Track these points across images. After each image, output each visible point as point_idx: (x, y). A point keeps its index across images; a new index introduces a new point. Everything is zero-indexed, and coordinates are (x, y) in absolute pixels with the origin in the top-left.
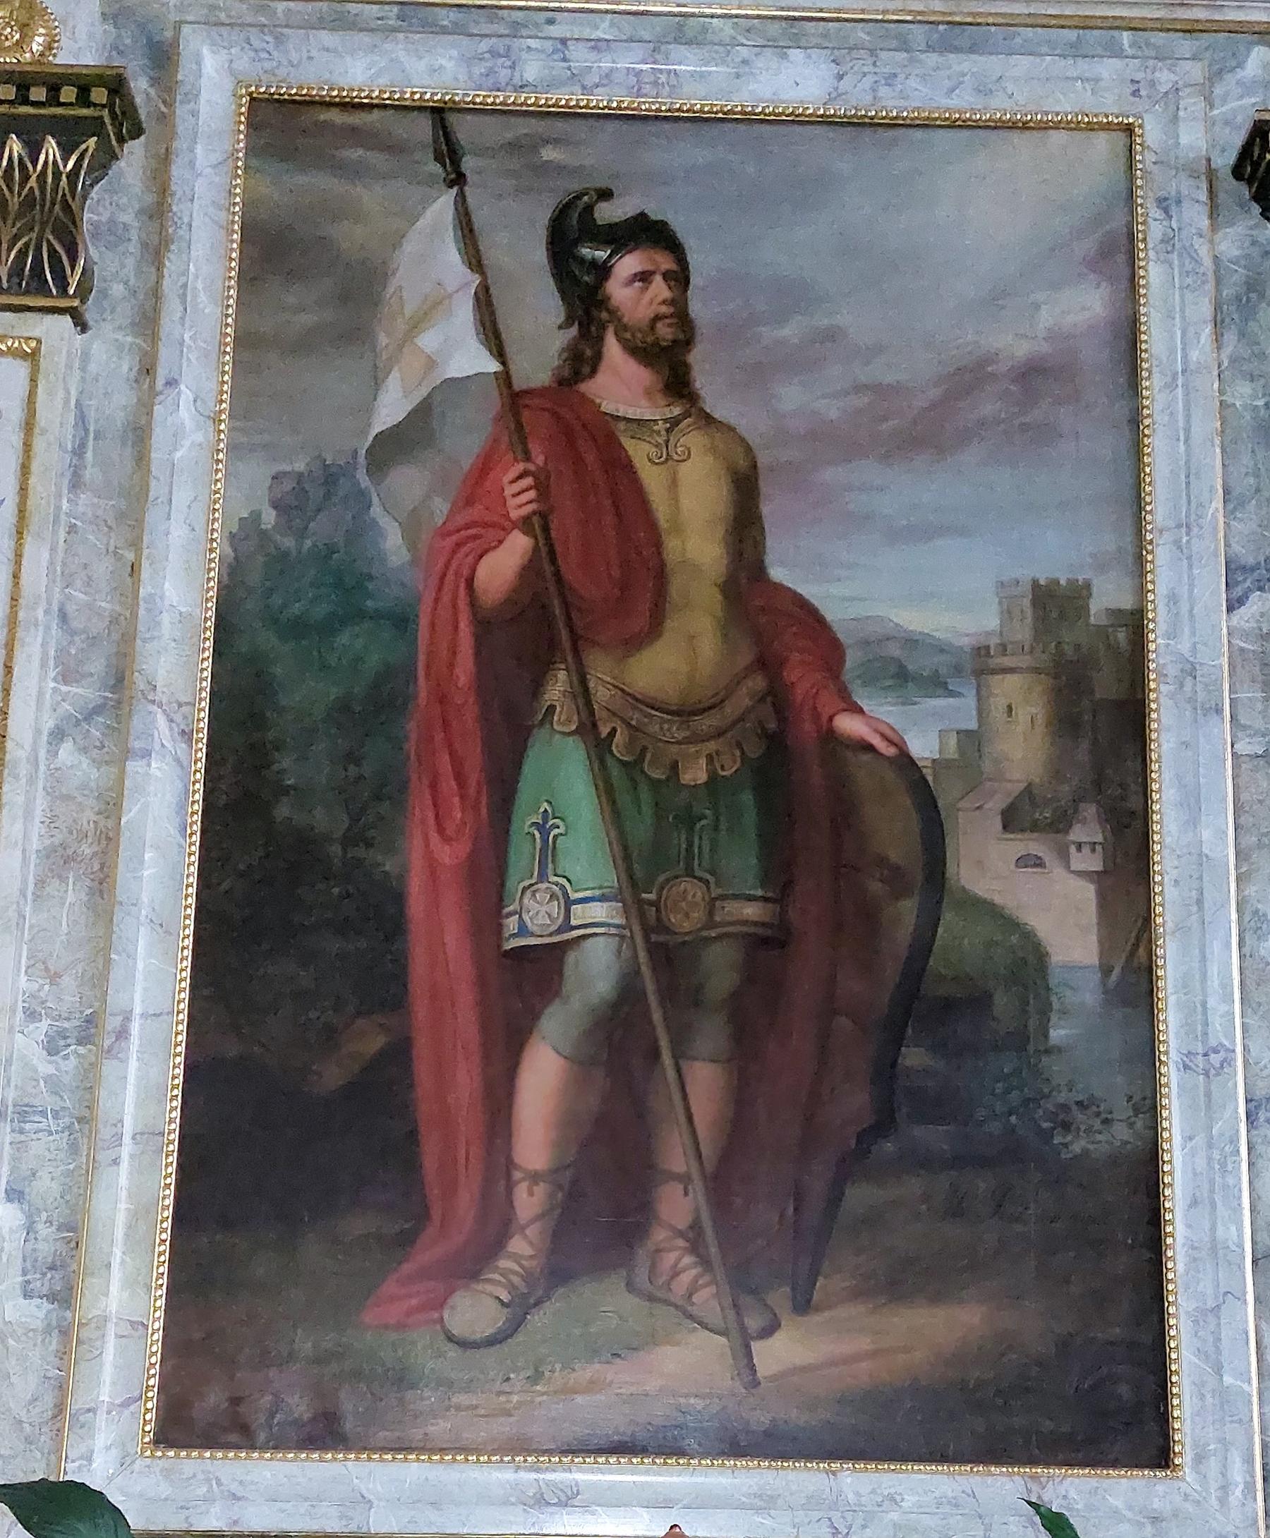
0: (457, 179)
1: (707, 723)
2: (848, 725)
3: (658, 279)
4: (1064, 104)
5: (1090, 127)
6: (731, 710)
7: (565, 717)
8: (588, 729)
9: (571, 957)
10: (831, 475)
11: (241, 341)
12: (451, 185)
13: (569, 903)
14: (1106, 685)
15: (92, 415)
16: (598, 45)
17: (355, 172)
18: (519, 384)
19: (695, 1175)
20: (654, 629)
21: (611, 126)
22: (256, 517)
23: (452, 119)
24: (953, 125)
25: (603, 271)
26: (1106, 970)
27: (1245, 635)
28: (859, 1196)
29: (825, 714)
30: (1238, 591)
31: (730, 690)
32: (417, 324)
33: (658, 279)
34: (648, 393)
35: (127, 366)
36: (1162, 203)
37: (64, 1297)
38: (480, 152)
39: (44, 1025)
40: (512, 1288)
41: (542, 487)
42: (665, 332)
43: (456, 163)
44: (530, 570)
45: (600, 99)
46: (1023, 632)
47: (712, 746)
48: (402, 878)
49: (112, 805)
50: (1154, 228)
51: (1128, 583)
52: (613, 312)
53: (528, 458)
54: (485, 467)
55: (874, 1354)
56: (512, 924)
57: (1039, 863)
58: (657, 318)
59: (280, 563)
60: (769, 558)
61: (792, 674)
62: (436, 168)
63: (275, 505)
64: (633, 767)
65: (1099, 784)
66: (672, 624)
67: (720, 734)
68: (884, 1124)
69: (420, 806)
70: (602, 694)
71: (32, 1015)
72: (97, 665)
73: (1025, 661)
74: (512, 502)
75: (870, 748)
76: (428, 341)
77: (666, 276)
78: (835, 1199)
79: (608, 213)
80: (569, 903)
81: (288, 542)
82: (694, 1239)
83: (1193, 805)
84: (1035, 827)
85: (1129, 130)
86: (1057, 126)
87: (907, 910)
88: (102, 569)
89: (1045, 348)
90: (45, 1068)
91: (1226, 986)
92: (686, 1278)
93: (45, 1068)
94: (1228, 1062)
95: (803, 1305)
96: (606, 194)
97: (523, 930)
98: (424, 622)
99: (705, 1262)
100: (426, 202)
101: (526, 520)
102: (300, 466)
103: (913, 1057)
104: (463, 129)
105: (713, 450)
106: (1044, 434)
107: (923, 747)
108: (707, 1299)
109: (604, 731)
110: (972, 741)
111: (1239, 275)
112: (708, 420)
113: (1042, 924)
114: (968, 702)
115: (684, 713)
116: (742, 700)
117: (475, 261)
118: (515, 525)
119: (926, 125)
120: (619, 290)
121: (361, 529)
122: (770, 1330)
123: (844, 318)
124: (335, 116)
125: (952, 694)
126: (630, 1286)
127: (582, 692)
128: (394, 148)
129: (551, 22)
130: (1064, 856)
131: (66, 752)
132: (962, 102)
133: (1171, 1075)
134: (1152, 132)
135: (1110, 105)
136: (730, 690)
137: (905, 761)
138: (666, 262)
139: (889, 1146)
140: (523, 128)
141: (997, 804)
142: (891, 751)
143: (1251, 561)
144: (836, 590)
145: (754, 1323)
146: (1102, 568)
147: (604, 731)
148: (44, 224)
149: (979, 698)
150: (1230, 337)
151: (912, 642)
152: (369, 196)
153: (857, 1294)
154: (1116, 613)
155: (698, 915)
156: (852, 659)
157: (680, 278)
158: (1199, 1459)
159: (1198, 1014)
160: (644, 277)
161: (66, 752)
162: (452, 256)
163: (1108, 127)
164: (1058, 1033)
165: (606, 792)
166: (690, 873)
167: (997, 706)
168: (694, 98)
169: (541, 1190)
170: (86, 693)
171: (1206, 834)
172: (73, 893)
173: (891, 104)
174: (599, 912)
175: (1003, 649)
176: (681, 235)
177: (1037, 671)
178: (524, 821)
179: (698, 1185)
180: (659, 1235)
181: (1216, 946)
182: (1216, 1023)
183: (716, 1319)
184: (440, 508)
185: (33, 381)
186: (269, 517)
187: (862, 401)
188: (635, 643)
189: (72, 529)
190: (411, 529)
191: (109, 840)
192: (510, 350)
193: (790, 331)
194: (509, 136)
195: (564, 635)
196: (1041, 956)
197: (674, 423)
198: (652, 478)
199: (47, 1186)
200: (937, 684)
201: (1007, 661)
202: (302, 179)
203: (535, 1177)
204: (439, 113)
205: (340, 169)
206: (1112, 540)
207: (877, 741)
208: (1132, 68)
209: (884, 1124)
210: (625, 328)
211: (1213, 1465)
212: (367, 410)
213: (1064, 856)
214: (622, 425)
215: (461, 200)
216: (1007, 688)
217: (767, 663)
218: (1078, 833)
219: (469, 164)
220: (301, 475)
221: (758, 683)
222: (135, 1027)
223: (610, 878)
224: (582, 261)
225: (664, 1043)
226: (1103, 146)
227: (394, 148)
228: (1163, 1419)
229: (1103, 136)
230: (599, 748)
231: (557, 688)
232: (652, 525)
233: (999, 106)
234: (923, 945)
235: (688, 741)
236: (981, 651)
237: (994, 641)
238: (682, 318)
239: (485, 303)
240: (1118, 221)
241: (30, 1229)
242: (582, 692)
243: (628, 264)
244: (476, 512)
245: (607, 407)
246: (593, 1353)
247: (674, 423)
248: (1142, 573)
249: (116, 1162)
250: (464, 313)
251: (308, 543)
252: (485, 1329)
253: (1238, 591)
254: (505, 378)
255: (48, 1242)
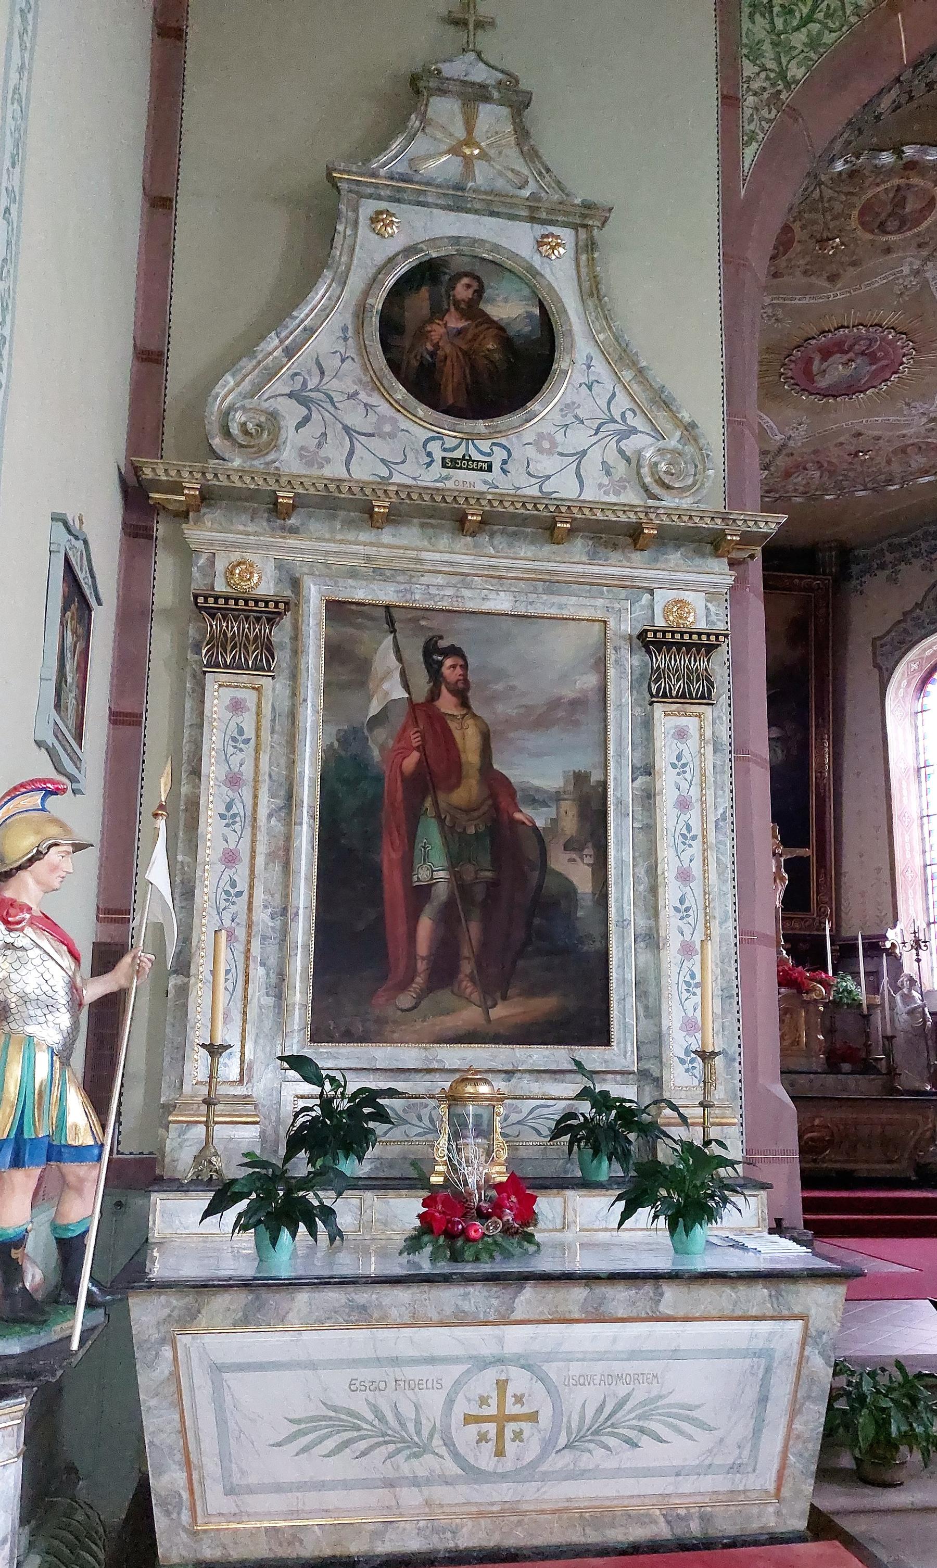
0: (394, 631)
1: (476, 814)
2: (518, 816)
3: (458, 668)
4: (585, 614)
5: (594, 621)
6: (481, 811)
7: (431, 812)
8: (438, 817)
9: (433, 889)
10: (512, 735)
11: (327, 685)
12: (391, 632)
13: (433, 871)
14: (595, 805)
15: (277, 708)
16: (439, 587)
17: (360, 627)
18: (415, 702)
19: (471, 956)
20: (458, 785)
21: (441, 615)
22: (332, 743)
23: (392, 610)
24: (550, 618)
25: (441, 664)
26: (594, 894)
27: (637, 790)
28: (521, 963)
29: (510, 812)
30: (635, 776)
31: (482, 804)
32: (382, 680)
33: (458, 668)
34: (456, 706)
35: (288, 692)
36: (615, 648)
37: (279, 996)
38: (401, 621)
39: (270, 910)
40: (415, 992)
41: (423, 738)
42: (460, 685)
43: (393, 625)
44: (420, 762)
45: (440, 605)
46: (571, 788)
47: (476, 822)
48: (382, 861)
49: (288, 838)
50: (612, 657)
51: (602, 771)
52: (444, 678)
53: (418, 726)
54: (404, 729)
55: (524, 1013)
56: (415, 878)
57: (574, 860)
58: (459, 680)
59: (340, 760)
60: (493, 761)
61: (501, 799)
62: (386, 626)
63: (338, 740)
64: (452, 828)
65: (592, 835)
66: (464, 781)
67: (479, 817)
68: (527, 942)
69: (386, 840)
70: (442, 805)
71: (266, 907)
72: (282, 793)
73: (571, 797)
74: (413, 741)
75: (524, 823)
76: (386, 686)
77: (461, 666)
78: (514, 963)
79: (443, 644)
80: (433, 871)
81: (343, 753)
82: (472, 979)
83: (620, 844)
84: (574, 849)
85: (605, 622)
86: (583, 620)
87: (536, 874)
88: (283, 761)
89: (579, 695)
90: (271, 924)
91: (629, 900)
92: (469, 990)
93: (271, 924)
94: (629, 924)
95: (504, 998)
96: (441, 638)
97: (419, 880)
98: (386, 780)
99: (474, 983)
100: (385, 637)
101: (418, 747)
102: (346, 727)
103: (537, 921)
104: (396, 614)
105: (476, 725)
106: (577, 723)
107: (540, 823)
108: (475, 997)
109: (443, 817)
110: (554, 821)
111: (638, 672)
112: (474, 716)
113: (575, 880)
114: (554, 809)
115: (467, 811)
116: (485, 808)
117: (400, 659)
118: (414, 749)
119: (542, 617)
120: (446, 671)
121: (366, 747)
122: (494, 1006)
123: (516, 683)
124: (354, 607)
125: (549, 807)
126: (452, 992)
127: (436, 803)
128: (372, 618)
129: (422, 576)
130: (582, 860)
131: (273, 821)
132: (553, 611)
133: (613, 928)
134: (612, 624)
135: (599, 615)
136: (482, 804)
137: (535, 828)
138: (461, 662)
139: (530, 949)
140: (414, 614)
141: (562, 841)
142: (530, 825)
143: (639, 766)
144: (517, 772)
145: (489, 1003)
146: (594, 767)
147: (443, 817)
148: (262, 646)
149: (557, 809)
150: (635, 692)
151: (538, 790)
152: (366, 636)
153: (520, 995)
154: (598, 782)
155: (473, 875)
156: (519, 794)
157: (465, 667)
158: (618, 1043)
159: (620, 909)
160: (454, 666)
161: (273, 821)
162: (393, 657)
163: (599, 621)
164: (580, 913)
165: (445, 837)
166: (470, 862)
167: (562, 811)
168: (471, 606)
169: (425, 962)
170: (280, 802)
171: (624, 854)
172: (278, 868)
173: (532, 611)
174: (442, 874)
175: (564, 792)
176: (466, 655)
177: (574, 800)
178: (419, 845)
179: (472, 962)
180: (461, 976)
181: (626, 889)
182: (626, 912)
183: (478, 1003)
184: (391, 743)
185: (259, 699)
186: (336, 744)
187: (522, 710)
188: (452, 788)
189: (272, 747)
190: (382, 748)
191: (287, 850)
192: (412, 690)
193: (500, 687)
194: (409, 616)
195: (430, 785)
196: (575, 890)
197: (464, 716)
198: (457, 735)
199: (272, 961)
200: (544, 804)
201: (565, 797)
202: (344, 629)
203: (423, 958)
204: (387, 607)
205: (351, 624)
206: (598, 759)
207: (526, 821)
208: (607, 603)
209: (527, 942)
210: (449, 683)
211: (622, 1045)
212: (367, 709)
213: (582, 860)
214: (447, 717)
215: (395, 637)
216: (566, 805)
217: (493, 796)
218: (586, 852)
219: (397, 625)
220: (345, 731)
221: (490, 802)
222: (301, 911)
223: (446, 864)
224: (433, 660)
225: (462, 915)
226: (597, 626)
227: (372, 618)
228: (608, 1032)
229: (597, 623)
230: (441, 821)
231: (428, 803)
232: (458, 750)
233: (566, 613)
234: (540, 887)
235: (469, 820)
236: (558, 792)
237: (562, 790)
238: (466, 681)
239: (403, 674)
240: (601, 654)
241: (268, 974)
242: (436, 803)
243: (448, 662)
244: (402, 744)
245: (443, 710)
246: (441, 1014)
247: (464, 716)
248: (606, 770)
249: (296, 954)
250: (397, 675)
251: (349, 754)
252: (407, 1006)
253: (635, 776)
254: (410, 700)
255: (273, 979)
